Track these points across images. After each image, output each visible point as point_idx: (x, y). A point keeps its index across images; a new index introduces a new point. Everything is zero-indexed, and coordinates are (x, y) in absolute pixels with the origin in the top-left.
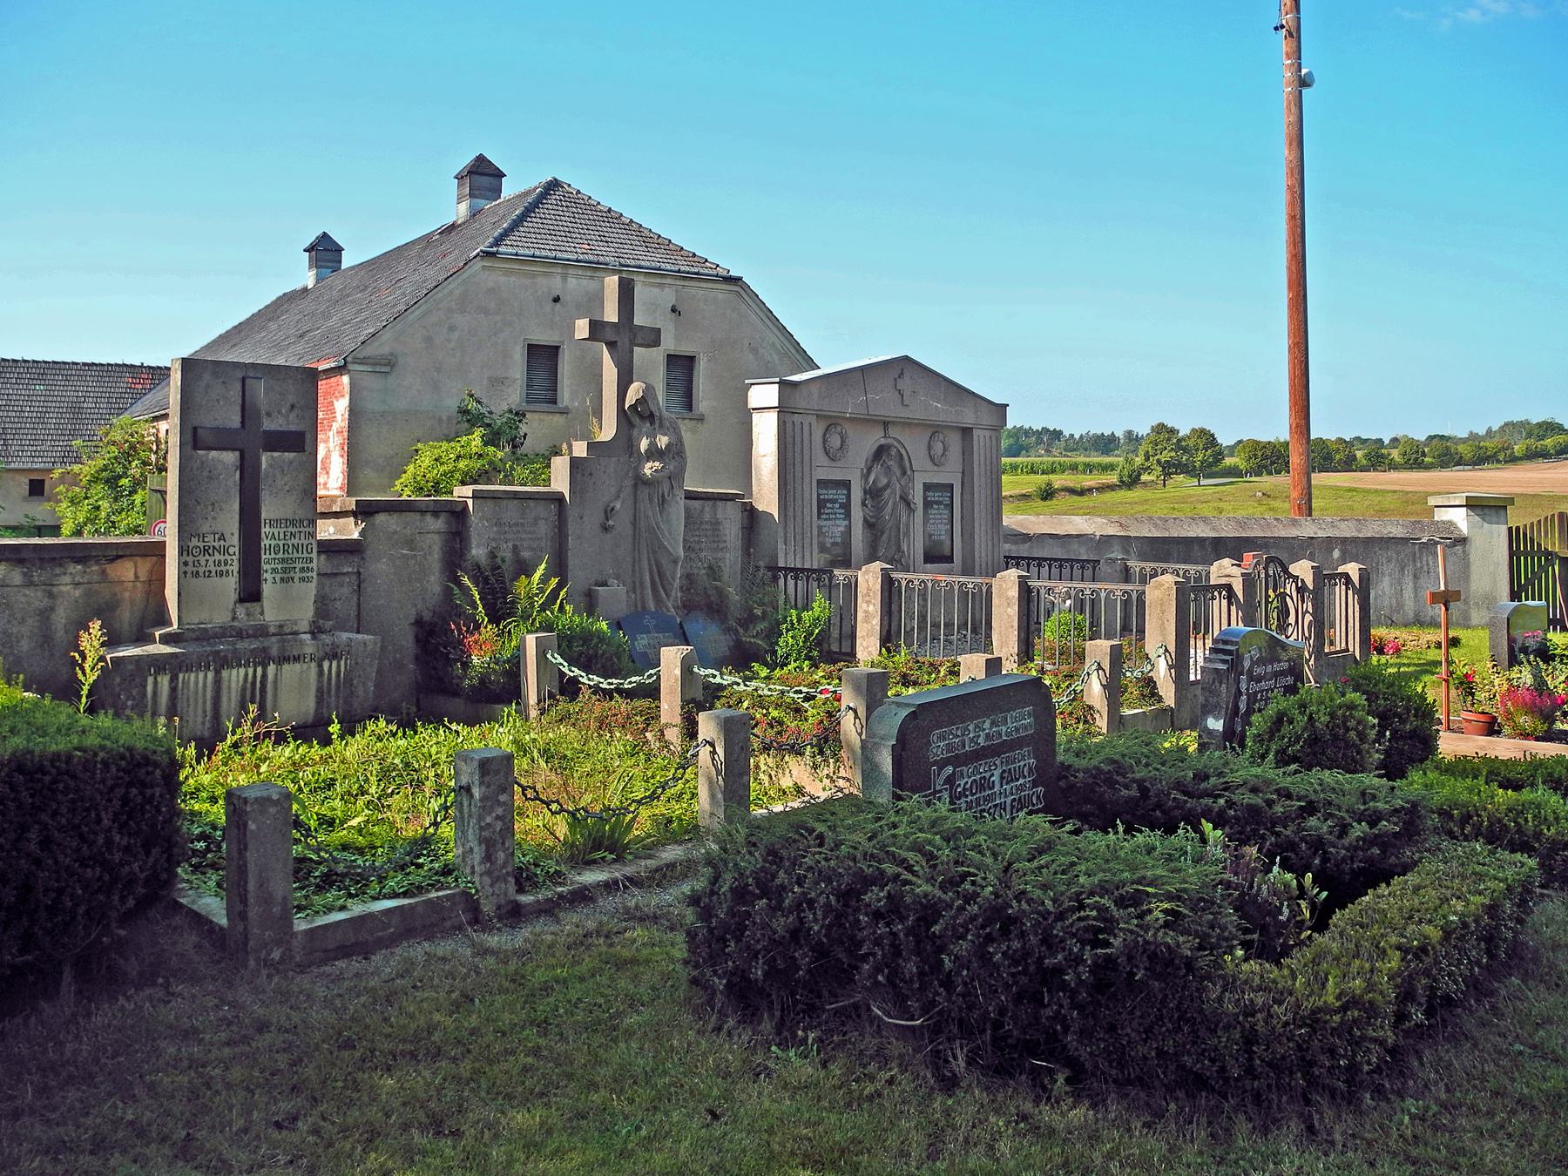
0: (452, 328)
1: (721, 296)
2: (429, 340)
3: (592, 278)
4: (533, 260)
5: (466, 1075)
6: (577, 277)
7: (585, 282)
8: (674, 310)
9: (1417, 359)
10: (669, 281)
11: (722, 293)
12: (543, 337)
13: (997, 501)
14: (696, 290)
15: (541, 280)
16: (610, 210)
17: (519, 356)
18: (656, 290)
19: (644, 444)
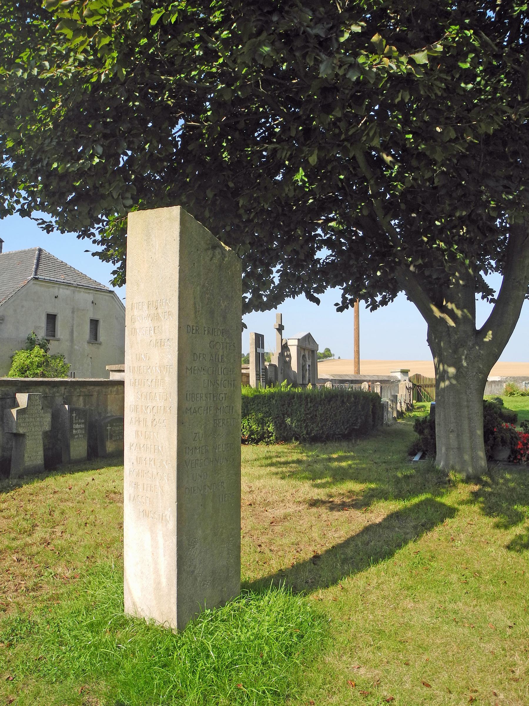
0: (23, 307)
1: (107, 298)
2: (15, 311)
3: (67, 289)
4: (50, 282)
5: (324, 427)
6: (63, 288)
7: (65, 291)
8: (93, 303)
9: (23, 233)
10: (91, 291)
11: (107, 296)
12: (52, 311)
13: (72, 428)
14: (100, 295)
15: (51, 289)
16: (62, 262)
17: (44, 319)
18: (87, 295)
19: (286, 354)
